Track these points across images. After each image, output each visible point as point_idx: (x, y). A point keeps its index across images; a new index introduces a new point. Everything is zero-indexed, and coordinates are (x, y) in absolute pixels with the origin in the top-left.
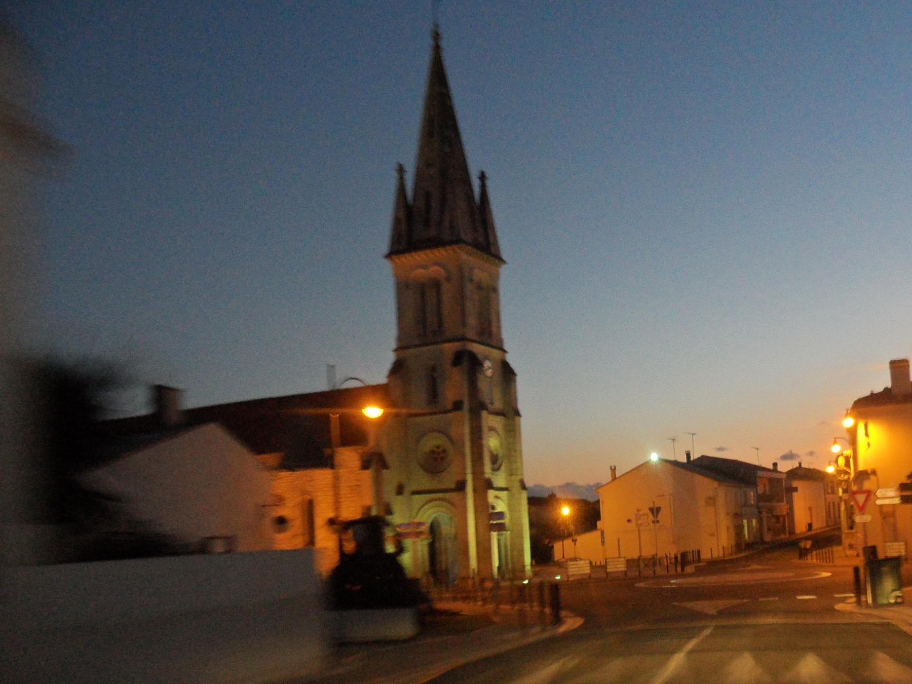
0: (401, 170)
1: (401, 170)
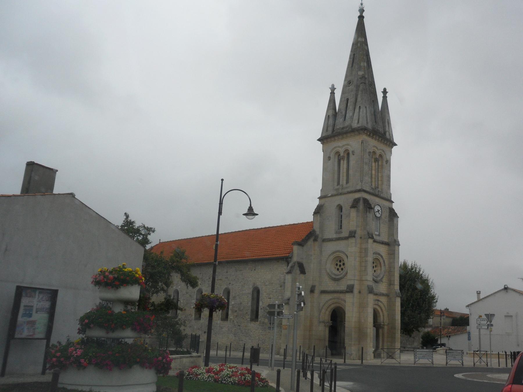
0: (333, 89)
1: (333, 89)
